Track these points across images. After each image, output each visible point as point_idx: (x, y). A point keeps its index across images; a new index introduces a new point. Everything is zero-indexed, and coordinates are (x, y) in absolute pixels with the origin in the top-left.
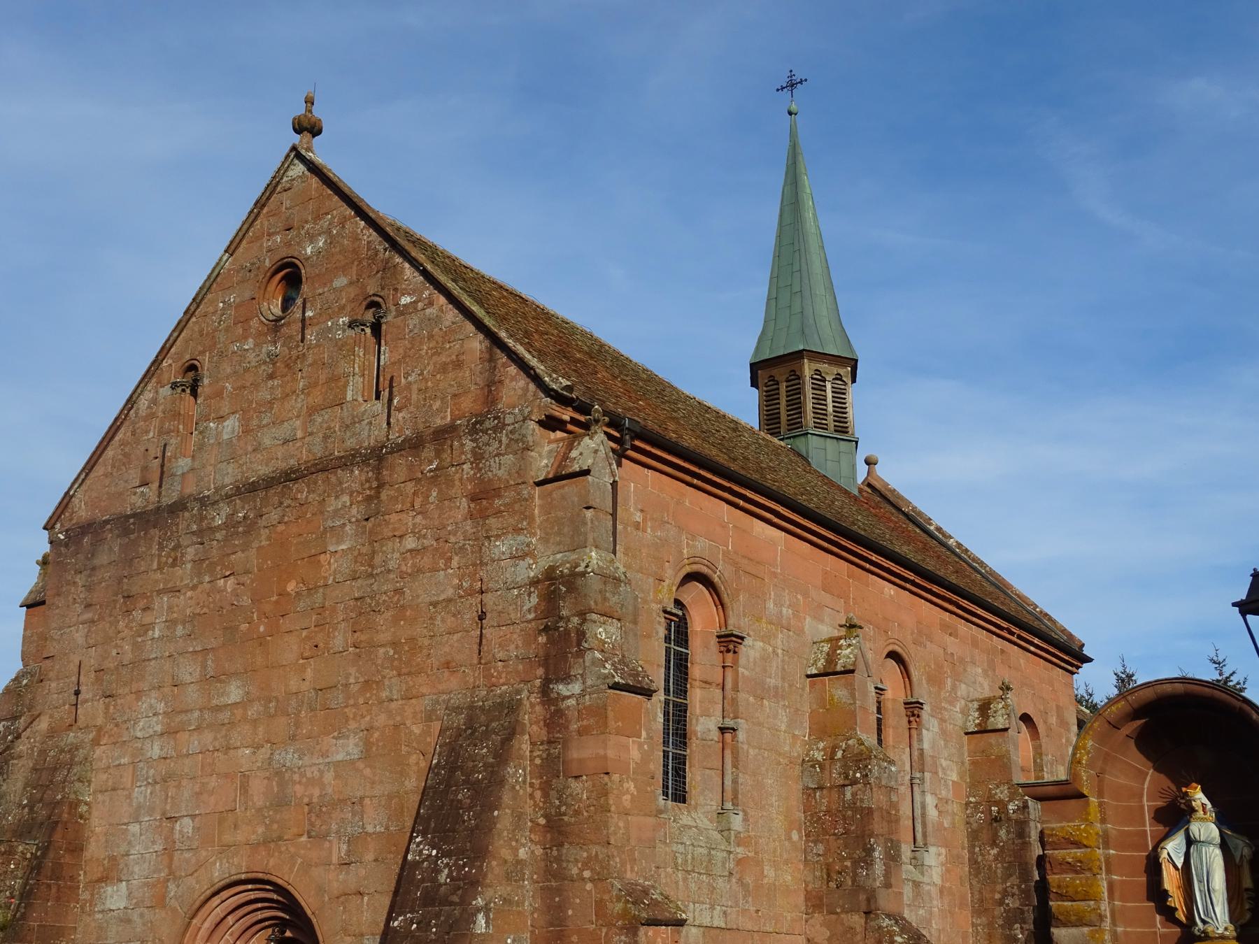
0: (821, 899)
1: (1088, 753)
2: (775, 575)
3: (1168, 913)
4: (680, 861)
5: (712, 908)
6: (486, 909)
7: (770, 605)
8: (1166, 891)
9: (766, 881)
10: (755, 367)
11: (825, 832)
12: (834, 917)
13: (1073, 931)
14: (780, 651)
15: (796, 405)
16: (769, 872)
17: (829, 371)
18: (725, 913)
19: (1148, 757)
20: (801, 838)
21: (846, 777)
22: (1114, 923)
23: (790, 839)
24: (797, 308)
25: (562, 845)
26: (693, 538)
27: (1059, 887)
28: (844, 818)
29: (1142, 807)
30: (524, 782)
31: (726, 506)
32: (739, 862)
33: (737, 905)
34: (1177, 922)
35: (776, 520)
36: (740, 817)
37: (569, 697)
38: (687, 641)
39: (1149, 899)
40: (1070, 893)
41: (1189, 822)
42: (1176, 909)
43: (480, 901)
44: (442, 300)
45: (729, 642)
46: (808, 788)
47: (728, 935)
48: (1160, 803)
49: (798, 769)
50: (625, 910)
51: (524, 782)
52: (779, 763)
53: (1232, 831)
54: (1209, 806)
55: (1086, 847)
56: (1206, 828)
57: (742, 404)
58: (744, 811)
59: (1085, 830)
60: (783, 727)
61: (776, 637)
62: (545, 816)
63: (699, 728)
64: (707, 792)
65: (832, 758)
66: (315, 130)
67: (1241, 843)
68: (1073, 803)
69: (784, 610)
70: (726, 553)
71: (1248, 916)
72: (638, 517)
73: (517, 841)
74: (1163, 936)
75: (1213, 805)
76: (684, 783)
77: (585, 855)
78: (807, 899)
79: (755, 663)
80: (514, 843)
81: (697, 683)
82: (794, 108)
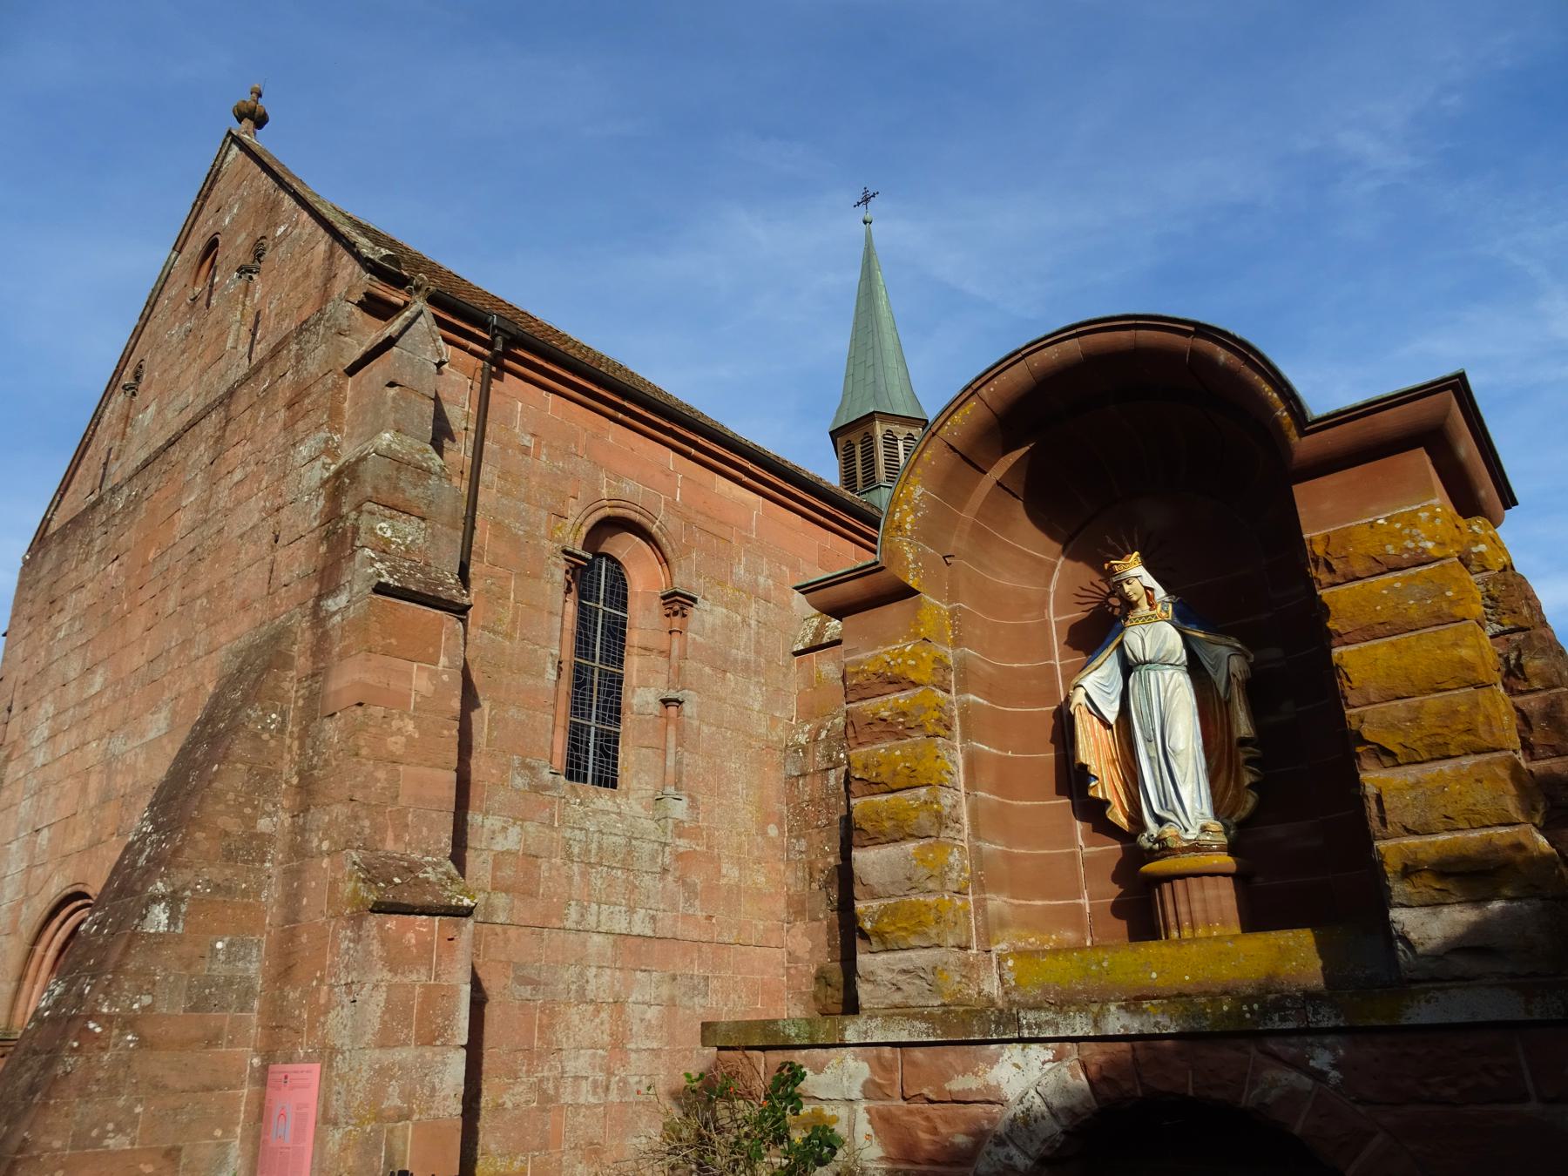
0: (803, 904)
1: (915, 510)
2: (748, 541)
3: (1093, 812)
4: (576, 850)
5: (631, 910)
6: (173, 900)
7: (740, 570)
8: (1084, 767)
9: (723, 881)
10: (834, 434)
11: (808, 825)
12: (816, 924)
13: (890, 851)
14: (753, 623)
15: (869, 463)
16: (730, 872)
17: (901, 431)
18: (653, 918)
19: (1052, 534)
20: (781, 834)
21: (830, 760)
22: (976, 833)
23: (764, 834)
24: (870, 379)
25: (308, 810)
26: (618, 478)
27: (866, 767)
28: (828, 806)
29: (1046, 624)
30: (281, 730)
31: (672, 453)
32: (679, 857)
33: (674, 907)
34: (1112, 830)
35: (746, 479)
36: (685, 802)
37: (335, 613)
38: (625, 605)
39: (1060, 791)
40: (884, 777)
41: (1123, 628)
42: (1107, 803)
43: (160, 887)
44: (305, 215)
45: (677, 602)
46: (791, 777)
47: (657, 945)
48: (1078, 615)
49: (778, 756)
50: (355, 892)
51: (281, 730)
52: (750, 746)
53: (1207, 630)
54: (1160, 593)
55: (914, 684)
56: (1156, 635)
57: (826, 469)
58: (690, 796)
59: (913, 654)
60: (757, 707)
61: (746, 606)
62: (299, 773)
63: (635, 701)
64: (641, 775)
65: (815, 740)
66: (260, 121)
67: (1224, 651)
68: (894, 610)
69: (761, 580)
70: (671, 505)
71: (1251, 800)
72: (528, 441)
73: (255, 808)
74: (1088, 862)
75: (1169, 592)
76: (615, 765)
77: (327, 818)
78: (788, 905)
79: (713, 630)
80: (248, 811)
81: (635, 650)
82: (868, 217)
